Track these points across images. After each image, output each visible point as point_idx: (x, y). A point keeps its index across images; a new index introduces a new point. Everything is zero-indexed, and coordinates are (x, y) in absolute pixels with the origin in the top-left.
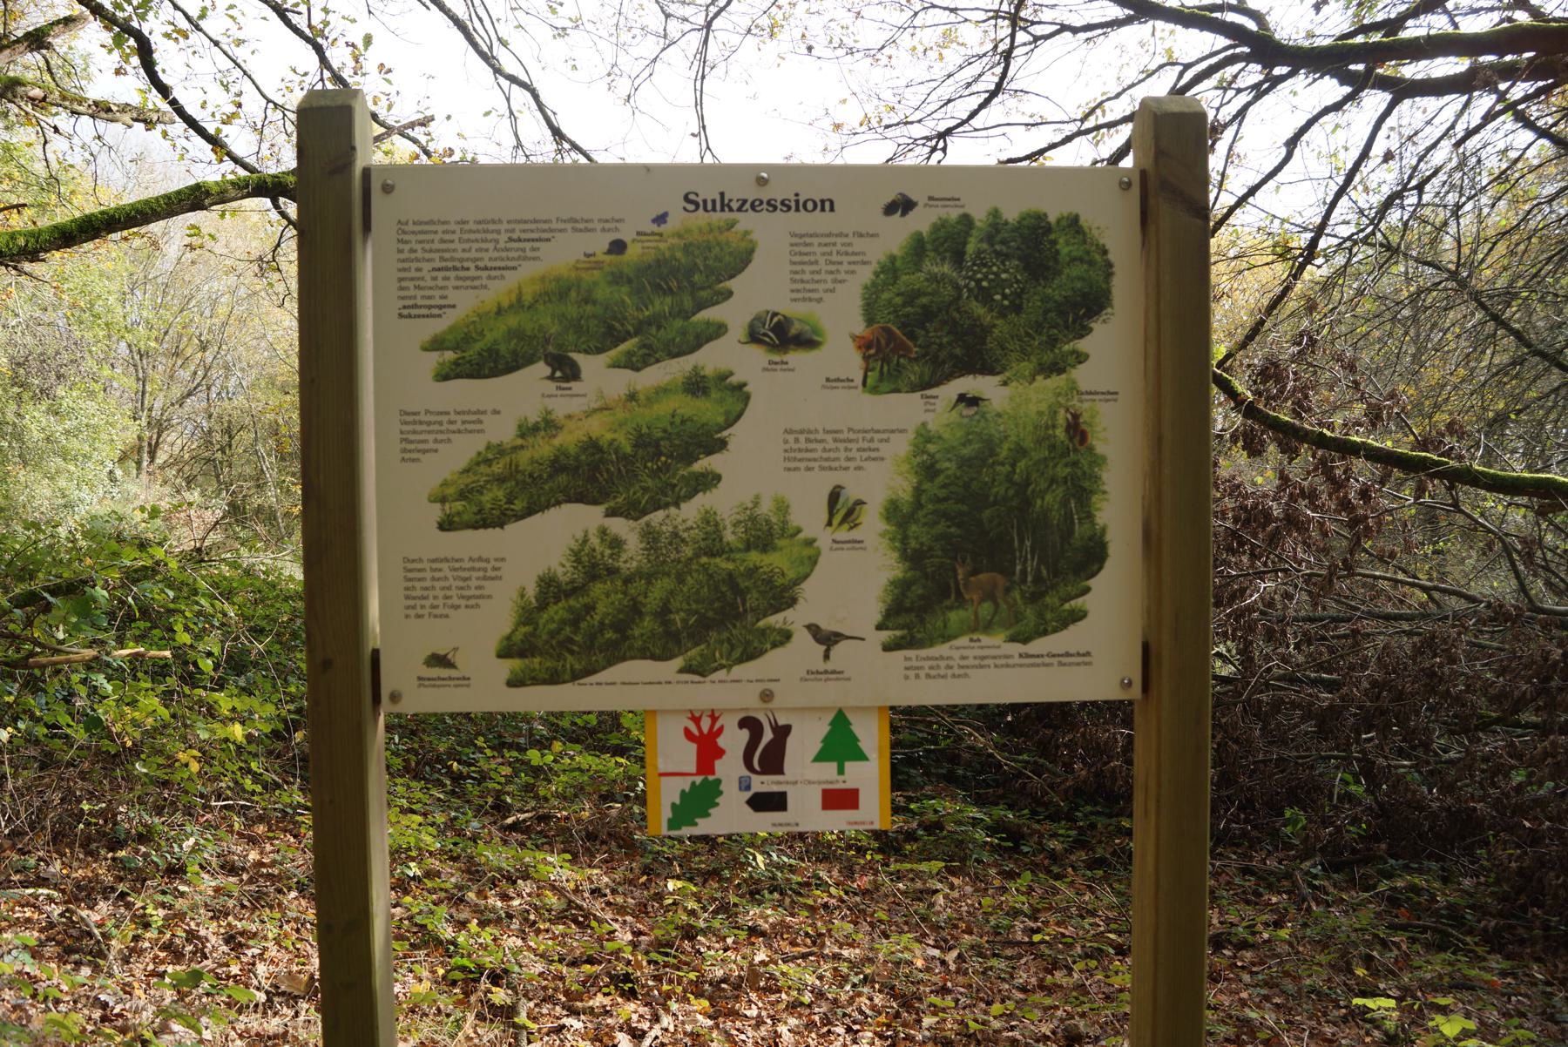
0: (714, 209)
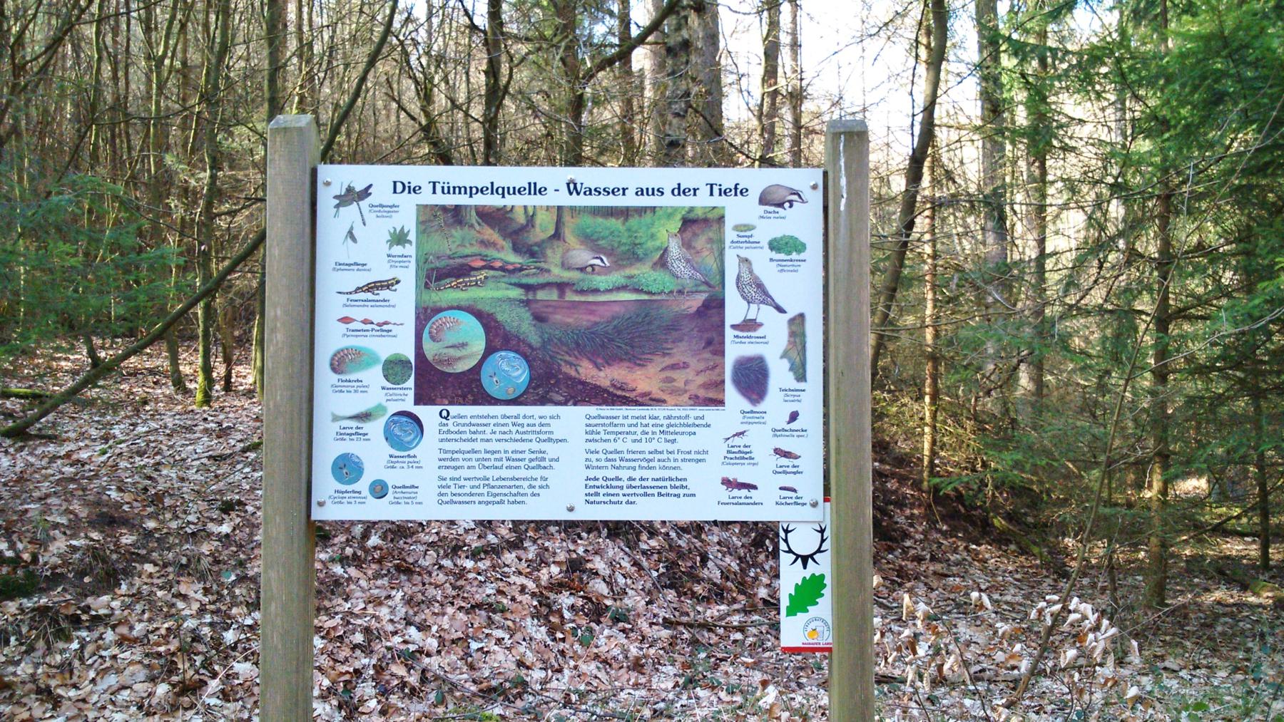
0: (449, 192)
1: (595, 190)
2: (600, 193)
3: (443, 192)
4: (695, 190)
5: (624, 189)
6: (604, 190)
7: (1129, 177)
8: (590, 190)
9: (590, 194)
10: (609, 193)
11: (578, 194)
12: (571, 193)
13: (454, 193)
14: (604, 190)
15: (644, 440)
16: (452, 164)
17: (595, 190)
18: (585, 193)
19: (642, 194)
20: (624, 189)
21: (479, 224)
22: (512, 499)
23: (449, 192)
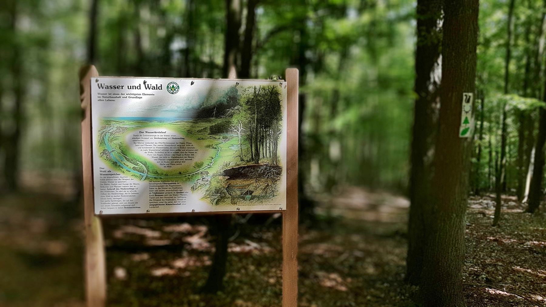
0: (131, 89)
1: (116, 88)
2: (112, 88)
3: (128, 88)
4: (122, 87)
5: (122, 87)
6: (114, 87)
7: (490, 213)
8: (108, 87)
9: (108, 88)
10: (116, 88)
11: (149, 89)
12: (146, 89)
13: (133, 89)
14: (114, 87)
15: (128, 97)
16: (281, 290)
17: (110, 87)
18: (106, 88)
19: (155, 89)
20: (122, 87)
21: (285, 88)
22: (107, 99)
23: (131, 89)
